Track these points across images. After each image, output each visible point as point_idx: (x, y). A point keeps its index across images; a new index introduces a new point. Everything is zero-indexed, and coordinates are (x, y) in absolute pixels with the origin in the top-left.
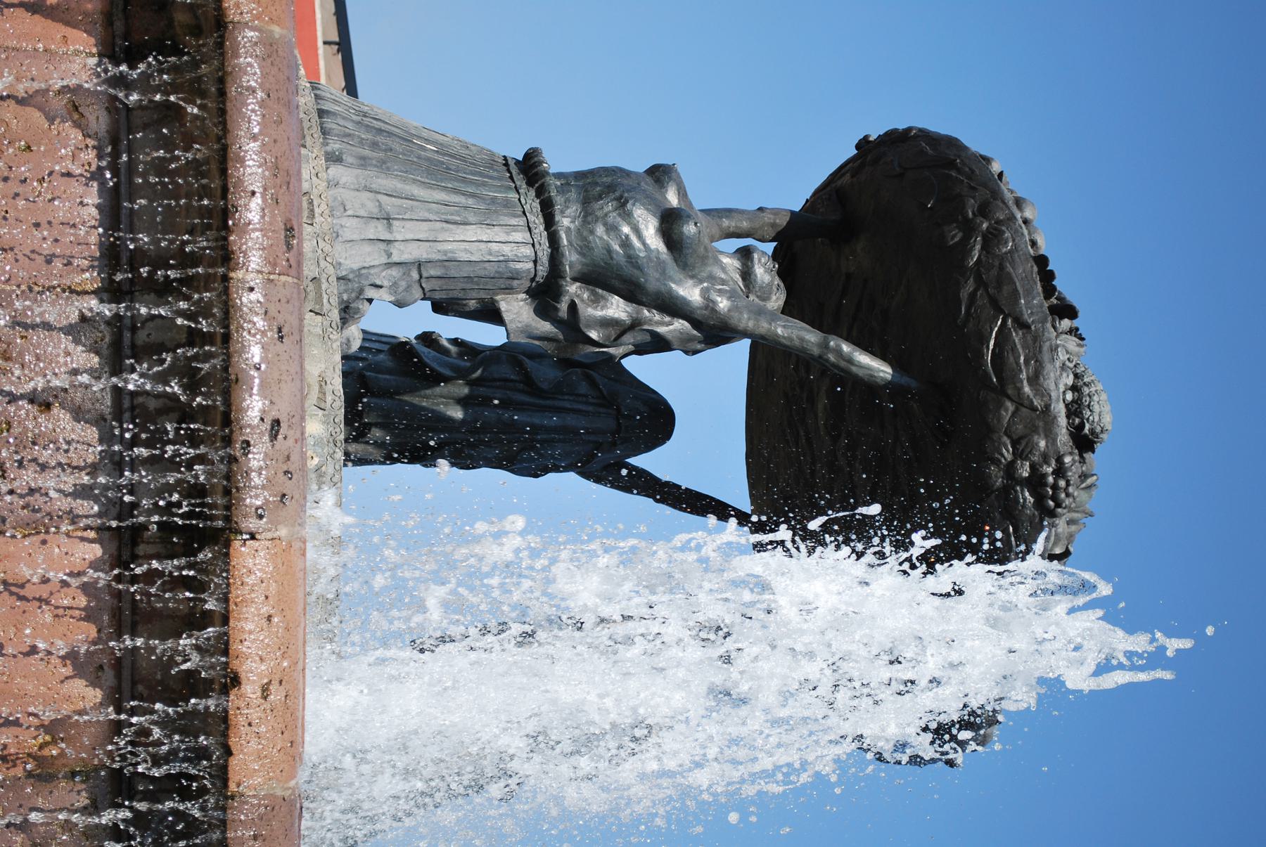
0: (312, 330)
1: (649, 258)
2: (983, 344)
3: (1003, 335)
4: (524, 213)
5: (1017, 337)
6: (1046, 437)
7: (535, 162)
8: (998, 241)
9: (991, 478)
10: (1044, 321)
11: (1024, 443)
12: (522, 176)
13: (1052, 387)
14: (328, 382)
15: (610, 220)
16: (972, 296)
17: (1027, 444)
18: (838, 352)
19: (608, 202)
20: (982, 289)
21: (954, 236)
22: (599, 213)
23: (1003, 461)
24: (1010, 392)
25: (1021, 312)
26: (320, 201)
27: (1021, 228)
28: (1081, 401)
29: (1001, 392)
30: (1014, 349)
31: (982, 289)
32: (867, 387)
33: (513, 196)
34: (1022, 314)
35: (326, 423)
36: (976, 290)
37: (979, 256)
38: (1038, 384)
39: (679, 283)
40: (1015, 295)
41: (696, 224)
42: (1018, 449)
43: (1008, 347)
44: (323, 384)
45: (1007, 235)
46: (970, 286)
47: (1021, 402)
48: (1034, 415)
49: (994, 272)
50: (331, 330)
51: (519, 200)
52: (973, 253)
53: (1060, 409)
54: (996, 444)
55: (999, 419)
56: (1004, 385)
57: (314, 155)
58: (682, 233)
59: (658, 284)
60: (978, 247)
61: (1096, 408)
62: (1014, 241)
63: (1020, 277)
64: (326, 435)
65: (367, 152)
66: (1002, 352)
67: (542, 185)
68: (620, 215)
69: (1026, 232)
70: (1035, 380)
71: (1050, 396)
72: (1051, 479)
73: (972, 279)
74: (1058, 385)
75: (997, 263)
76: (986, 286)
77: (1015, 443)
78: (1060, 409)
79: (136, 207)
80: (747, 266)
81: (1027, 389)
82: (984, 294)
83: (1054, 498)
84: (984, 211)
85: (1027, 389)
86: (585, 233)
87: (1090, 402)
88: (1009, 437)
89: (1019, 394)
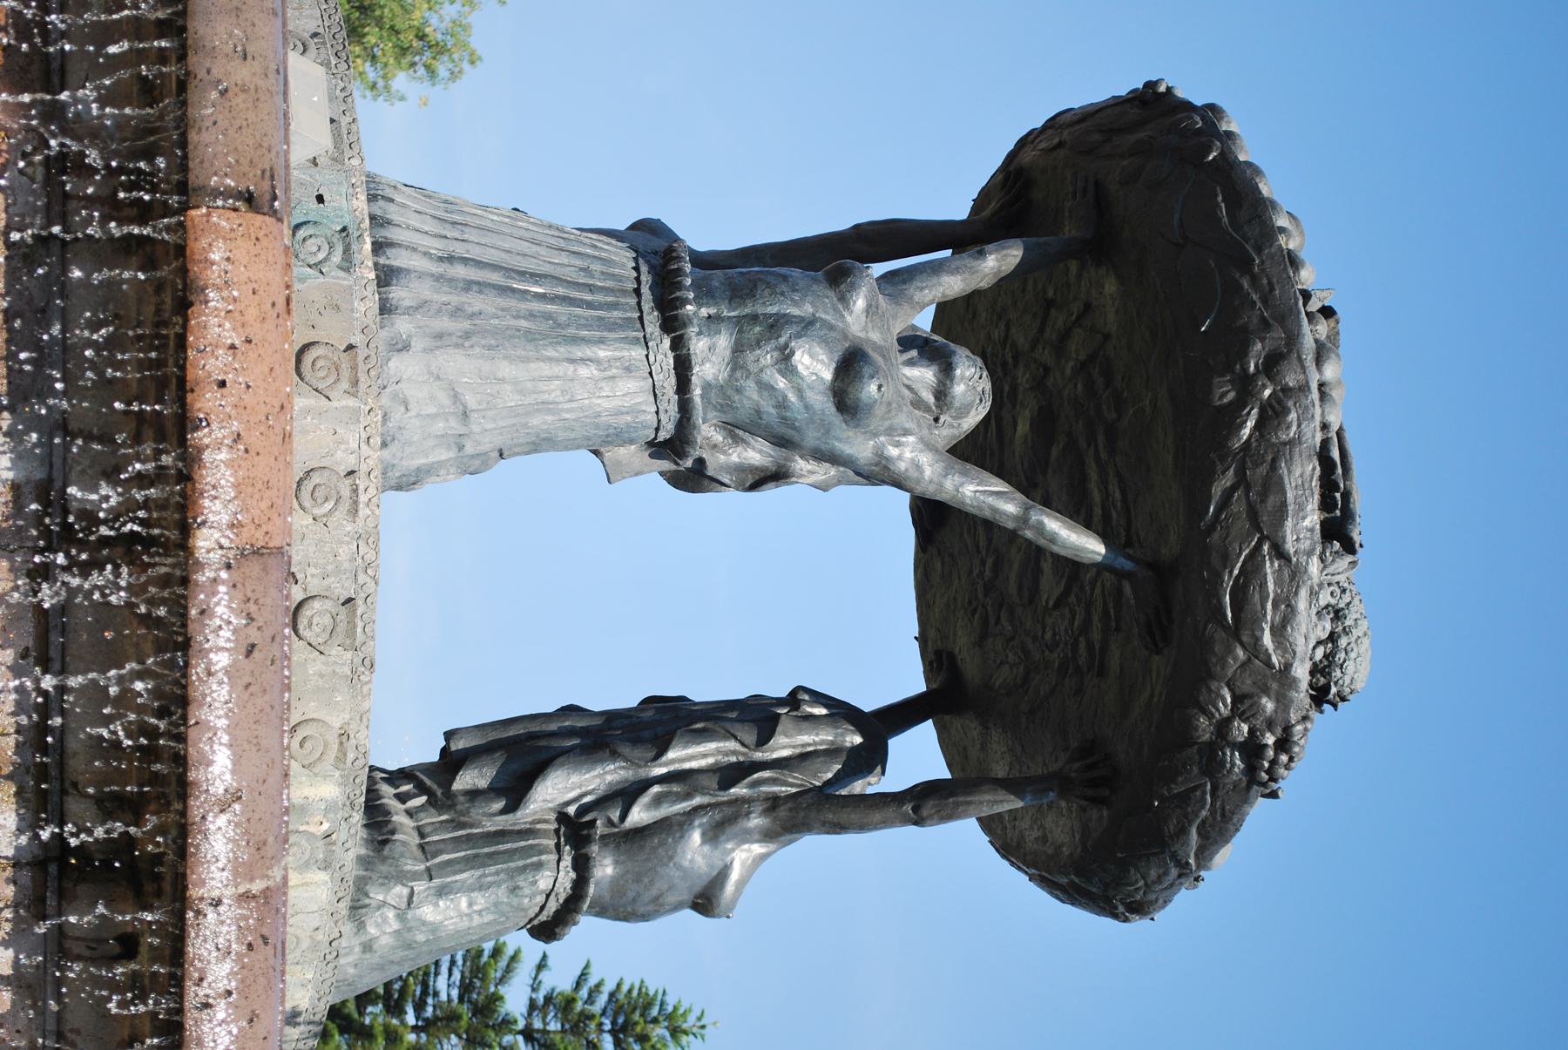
0: (337, 670)
1: (811, 421)
2: (1225, 567)
3: (1253, 568)
4: (651, 374)
5: (1270, 568)
6: (1278, 701)
7: (677, 298)
8: (1279, 424)
9: (1197, 730)
10: (1310, 553)
11: (1247, 703)
12: (656, 313)
13: (1300, 641)
14: (352, 736)
15: (765, 377)
16: (1228, 494)
17: (1251, 706)
18: (1040, 528)
19: (767, 352)
20: (1242, 488)
21: (1224, 394)
22: (753, 368)
23: (1217, 716)
24: (1245, 639)
25: (1284, 538)
26: (367, 483)
27: (1314, 406)
28: (1334, 657)
29: (1235, 632)
30: (1263, 585)
31: (1242, 488)
32: (1072, 567)
33: (638, 353)
34: (1284, 542)
35: (342, 784)
36: (1233, 489)
37: (1250, 436)
38: (1282, 635)
39: (847, 441)
40: (1281, 511)
41: (880, 387)
42: (1238, 709)
43: (1257, 583)
44: (345, 737)
45: (1293, 416)
46: (1227, 480)
47: (1255, 649)
48: (1268, 672)
49: (1263, 470)
50: (363, 669)
51: (647, 356)
52: (1243, 432)
53: (1301, 672)
54: (1213, 695)
55: (1224, 665)
56: (1243, 625)
57: (368, 408)
58: (859, 400)
59: (818, 442)
60: (1250, 424)
61: (1350, 666)
62: (1299, 426)
63: (1293, 485)
64: (341, 799)
65: (444, 324)
66: (1245, 586)
67: (681, 336)
68: (780, 372)
69: (1318, 411)
70: (1279, 632)
71: (1295, 654)
72: (1271, 753)
73: (1232, 470)
74: (1308, 631)
75: (1269, 458)
76: (1248, 488)
77: (1236, 699)
78: (1301, 672)
79: (101, 909)
80: (944, 385)
81: (1267, 640)
82: (1243, 498)
83: (1268, 772)
84: (1272, 364)
85: (1267, 640)
86: (730, 392)
87: (1344, 661)
88: (1231, 690)
89: (1255, 644)
